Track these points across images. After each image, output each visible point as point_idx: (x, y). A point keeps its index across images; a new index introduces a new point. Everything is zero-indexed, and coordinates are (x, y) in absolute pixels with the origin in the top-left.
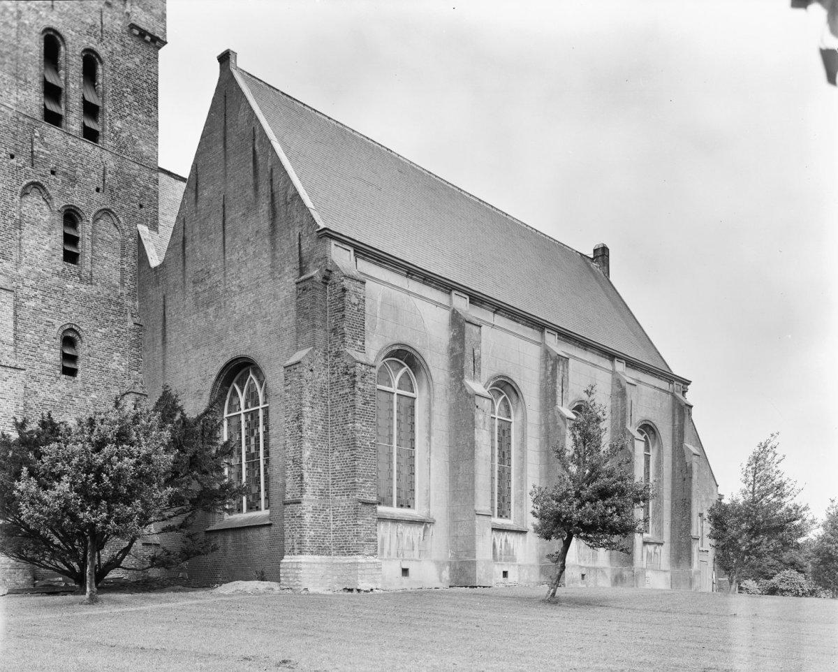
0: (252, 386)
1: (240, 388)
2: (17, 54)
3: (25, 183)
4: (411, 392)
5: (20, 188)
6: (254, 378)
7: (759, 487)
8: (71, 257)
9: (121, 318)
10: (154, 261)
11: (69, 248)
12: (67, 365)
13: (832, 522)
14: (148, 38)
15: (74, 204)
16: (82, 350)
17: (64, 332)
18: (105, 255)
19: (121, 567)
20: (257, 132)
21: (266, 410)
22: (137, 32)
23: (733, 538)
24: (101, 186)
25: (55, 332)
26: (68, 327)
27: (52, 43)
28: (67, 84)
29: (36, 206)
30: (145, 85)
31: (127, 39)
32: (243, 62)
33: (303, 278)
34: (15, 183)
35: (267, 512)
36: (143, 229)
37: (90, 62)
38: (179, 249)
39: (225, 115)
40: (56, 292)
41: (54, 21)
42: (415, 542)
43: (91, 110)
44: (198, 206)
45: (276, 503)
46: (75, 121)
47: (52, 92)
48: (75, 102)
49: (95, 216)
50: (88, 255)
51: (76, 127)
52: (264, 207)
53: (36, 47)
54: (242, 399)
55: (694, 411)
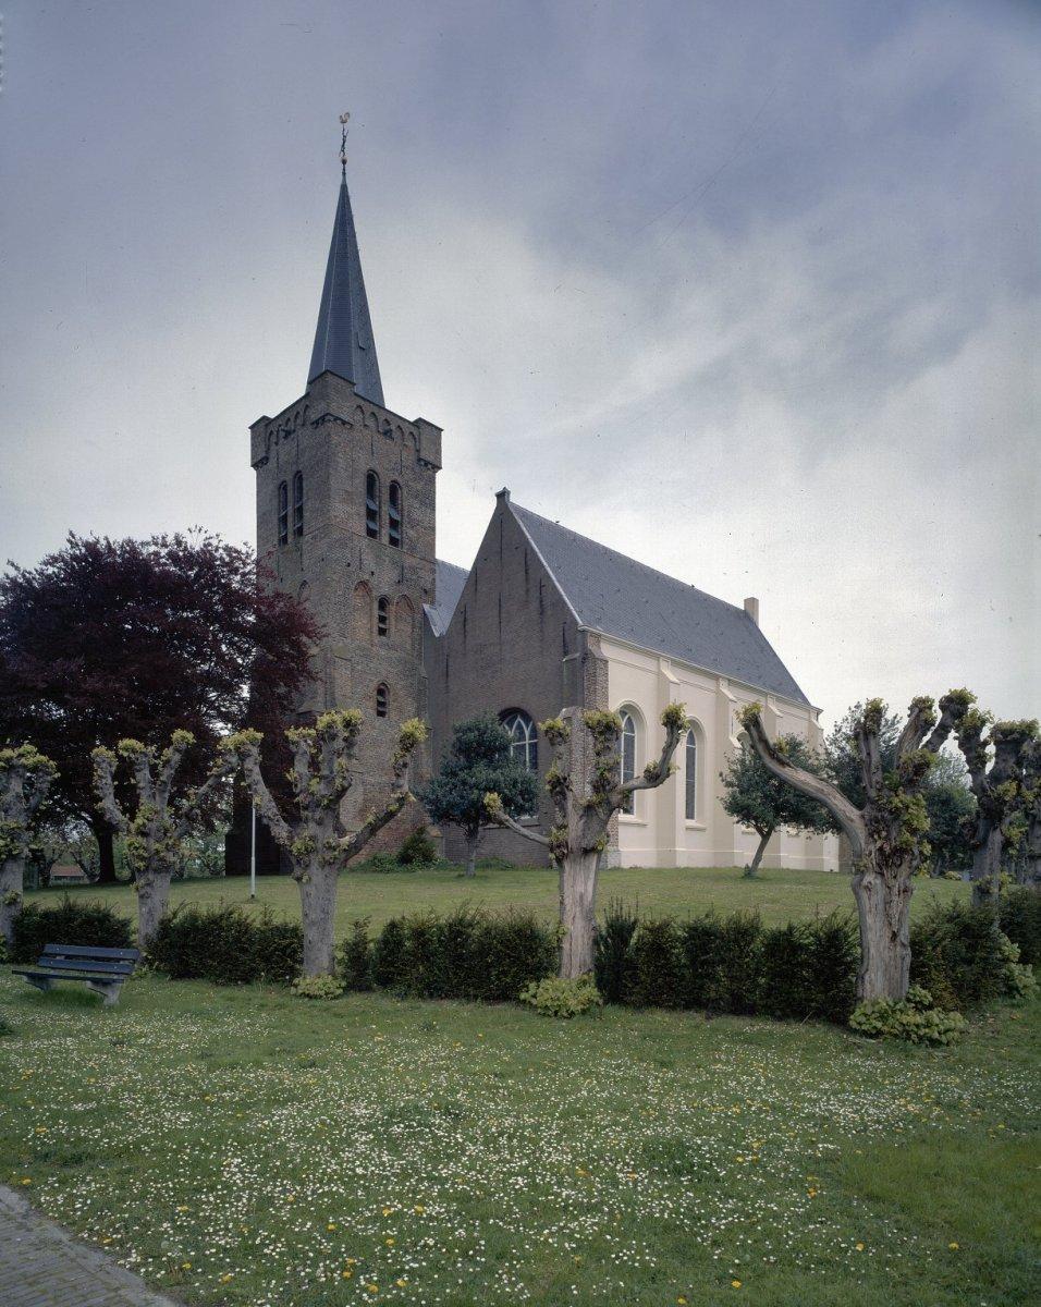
6: (522, 722)
8: (382, 632)
10: (438, 629)
11: (382, 626)
12: (380, 709)
14: (430, 466)
16: (390, 698)
19: (46, 955)
20: (529, 552)
22: (423, 463)
23: (921, 1011)
25: (374, 685)
27: (371, 479)
28: (380, 508)
31: (417, 469)
32: (514, 499)
36: (426, 607)
37: (394, 489)
38: (460, 626)
41: (375, 465)
42: (787, 769)
43: (394, 524)
47: (372, 515)
48: (386, 521)
50: (393, 630)
51: (385, 540)
52: (535, 605)
53: (360, 484)
54: (527, 733)
55: (767, 625)
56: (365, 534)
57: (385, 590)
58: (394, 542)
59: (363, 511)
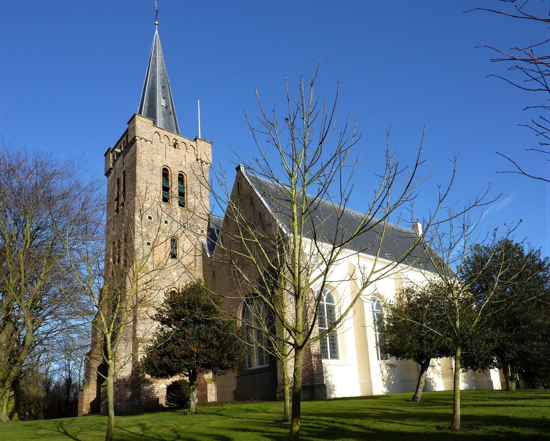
14: (204, 163)
43: (181, 194)
47: (166, 189)
58: (181, 205)
59: (160, 188)
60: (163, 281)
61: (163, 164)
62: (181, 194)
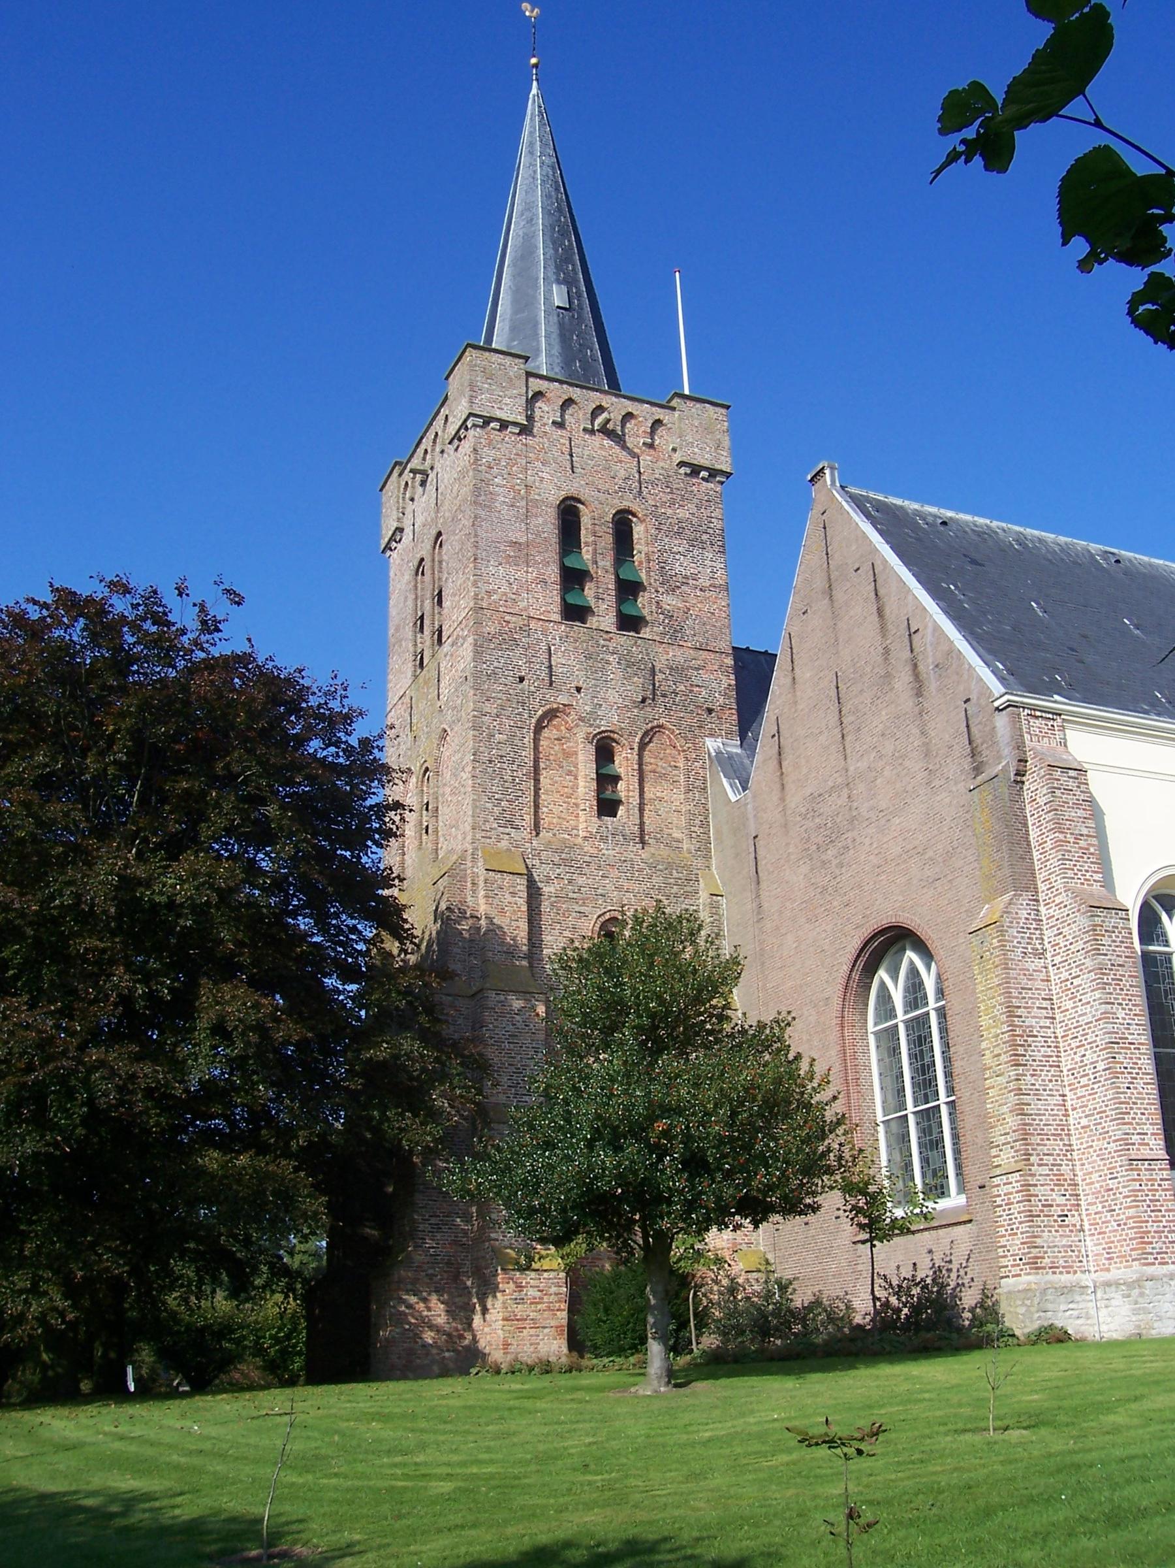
0: (914, 972)
1: (892, 977)
2: (149, 1092)
3: (540, 712)
4: (1165, 946)
5: (533, 721)
7: (464, 930)
8: (607, 806)
9: (688, 889)
13: (113, 899)
15: (603, 728)
17: (603, 924)
18: (658, 794)
21: (942, 1013)
24: (649, 694)
26: (607, 916)
29: (556, 742)
30: (705, 537)
33: (979, 778)
34: (526, 716)
35: (961, 1200)
39: (827, 554)
40: (588, 864)
43: (628, 589)
44: (798, 693)
45: (973, 1182)
46: (605, 617)
47: (573, 578)
49: (641, 739)
52: (903, 680)
53: (547, 524)
56: (557, 617)
57: (609, 720)
58: (630, 623)
60: (575, 896)
61: (563, 494)
62: (628, 589)
